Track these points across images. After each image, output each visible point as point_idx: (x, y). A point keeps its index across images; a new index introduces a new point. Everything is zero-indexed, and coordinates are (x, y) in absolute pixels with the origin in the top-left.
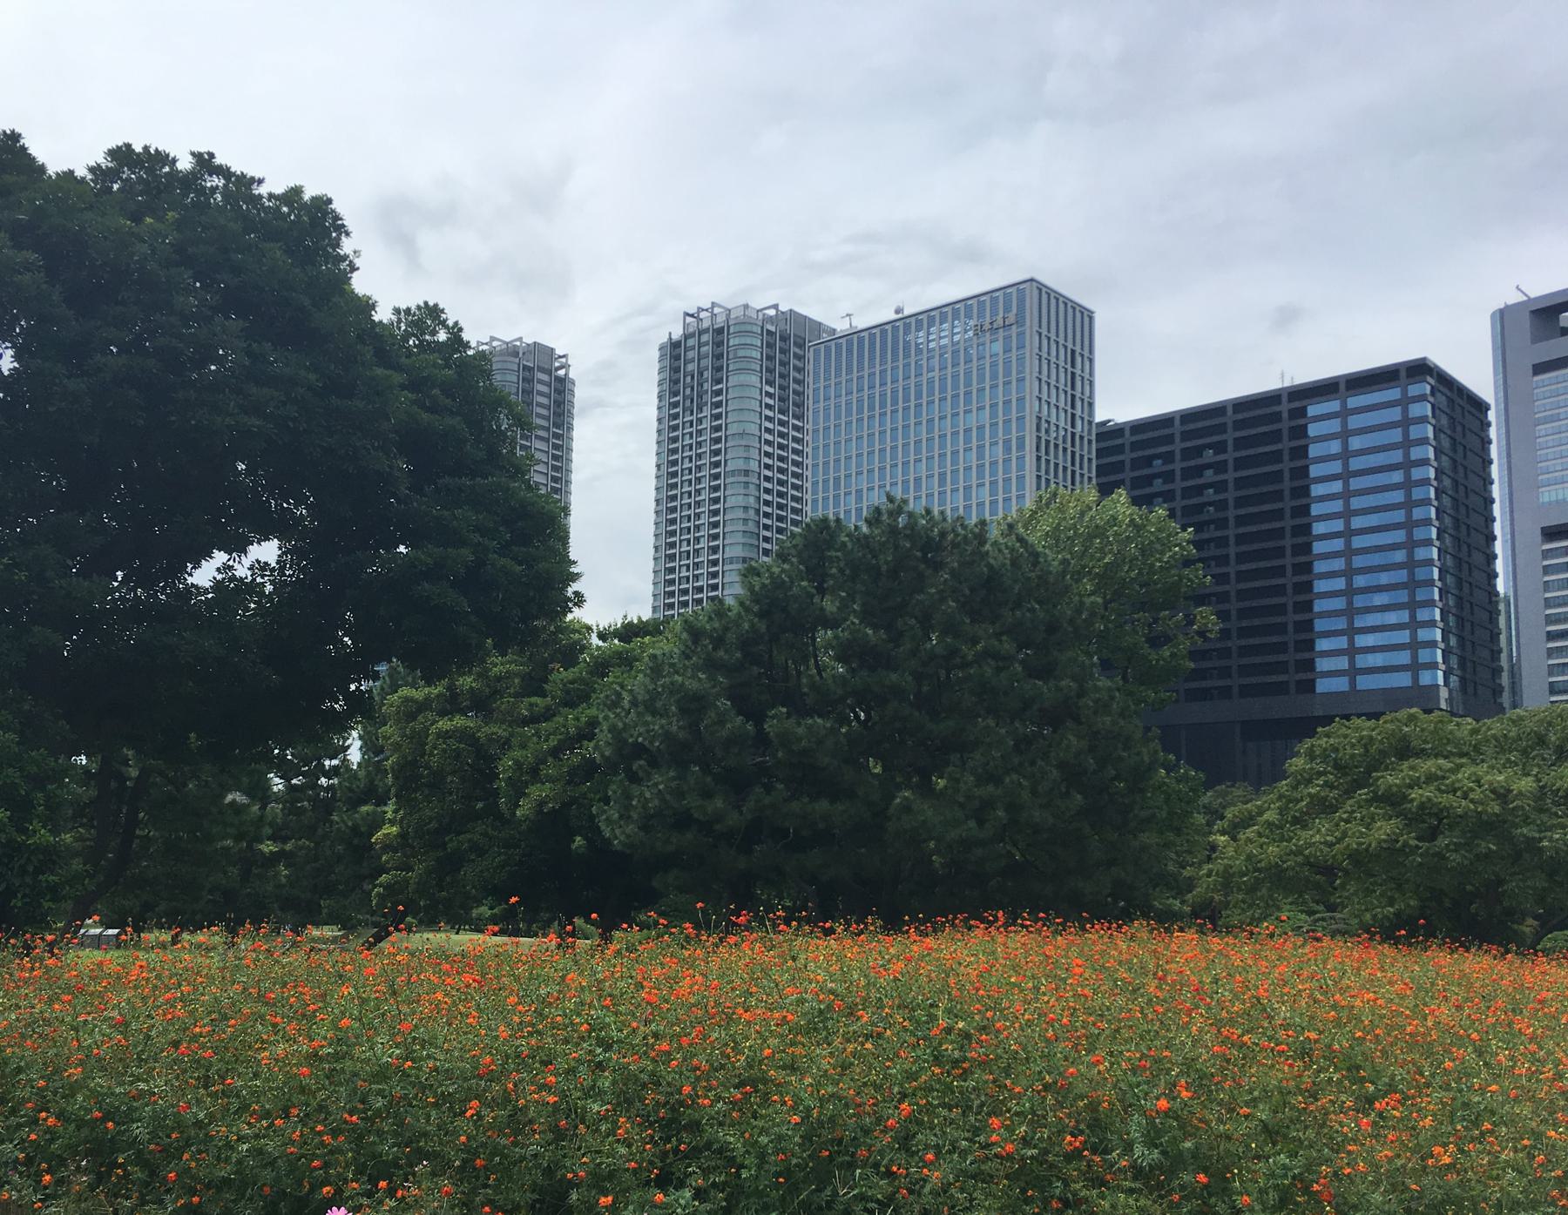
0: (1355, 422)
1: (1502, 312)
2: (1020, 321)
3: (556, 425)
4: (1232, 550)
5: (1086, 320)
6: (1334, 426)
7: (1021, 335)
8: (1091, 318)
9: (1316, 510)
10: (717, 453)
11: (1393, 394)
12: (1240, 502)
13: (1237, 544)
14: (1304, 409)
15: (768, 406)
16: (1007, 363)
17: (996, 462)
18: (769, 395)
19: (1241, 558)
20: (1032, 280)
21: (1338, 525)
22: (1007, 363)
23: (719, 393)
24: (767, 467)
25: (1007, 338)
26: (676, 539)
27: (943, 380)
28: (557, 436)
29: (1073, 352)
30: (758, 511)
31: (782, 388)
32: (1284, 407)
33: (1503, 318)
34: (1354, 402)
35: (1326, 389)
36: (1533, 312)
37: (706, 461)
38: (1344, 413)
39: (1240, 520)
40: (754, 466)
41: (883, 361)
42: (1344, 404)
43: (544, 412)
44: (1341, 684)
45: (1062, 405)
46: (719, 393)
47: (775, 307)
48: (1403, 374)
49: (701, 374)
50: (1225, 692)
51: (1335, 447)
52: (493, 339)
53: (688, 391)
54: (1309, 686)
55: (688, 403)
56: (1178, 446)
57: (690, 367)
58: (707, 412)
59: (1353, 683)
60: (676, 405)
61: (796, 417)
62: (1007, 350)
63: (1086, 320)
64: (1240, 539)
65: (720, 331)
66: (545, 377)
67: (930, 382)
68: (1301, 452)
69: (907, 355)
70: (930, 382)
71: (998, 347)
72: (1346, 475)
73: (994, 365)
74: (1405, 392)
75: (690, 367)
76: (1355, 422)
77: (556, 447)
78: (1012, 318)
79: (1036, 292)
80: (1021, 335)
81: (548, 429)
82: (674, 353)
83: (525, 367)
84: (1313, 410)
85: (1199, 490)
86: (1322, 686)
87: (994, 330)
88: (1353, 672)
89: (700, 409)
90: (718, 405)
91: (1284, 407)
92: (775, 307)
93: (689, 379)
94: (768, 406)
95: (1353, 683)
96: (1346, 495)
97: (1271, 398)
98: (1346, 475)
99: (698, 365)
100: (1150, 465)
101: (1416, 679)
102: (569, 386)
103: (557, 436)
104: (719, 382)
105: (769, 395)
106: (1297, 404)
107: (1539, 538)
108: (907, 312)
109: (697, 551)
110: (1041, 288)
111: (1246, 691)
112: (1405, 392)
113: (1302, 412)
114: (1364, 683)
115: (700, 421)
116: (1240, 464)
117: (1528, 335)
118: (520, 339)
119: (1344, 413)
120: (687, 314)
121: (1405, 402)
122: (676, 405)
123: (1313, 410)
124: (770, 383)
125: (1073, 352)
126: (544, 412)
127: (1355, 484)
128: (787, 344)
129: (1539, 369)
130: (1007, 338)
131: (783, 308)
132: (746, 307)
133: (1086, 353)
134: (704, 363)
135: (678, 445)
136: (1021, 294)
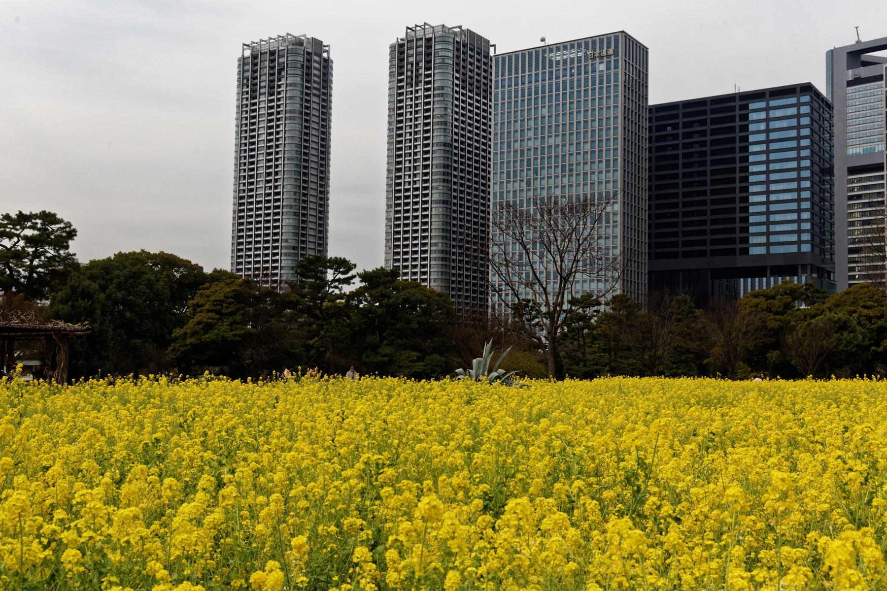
1: (832, 51)
2: (616, 53)
3: (324, 88)
4: (709, 178)
7: (616, 61)
8: (647, 52)
9: (752, 159)
11: (793, 100)
12: (713, 153)
13: (711, 175)
14: (747, 106)
15: (457, 85)
16: (608, 76)
17: (594, 131)
18: (457, 78)
19: (713, 182)
20: (623, 32)
21: (763, 168)
22: (608, 76)
25: (609, 63)
27: (572, 82)
28: (324, 94)
30: (301, 113)
31: (463, 74)
32: (737, 103)
33: (832, 55)
34: (773, 103)
36: (848, 53)
37: (421, 114)
39: (713, 162)
40: (450, 120)
41: (537, 68)
42: (768, 104)
44: (761, 251)
46: (429, 76)
47: (460, 27)
48: (798, 90)
50: (703, 254)
51: (763, 126)
52: (288, 34)
53: (409, 73)
54: (745, 251)
56: (681, 121)
57: (410, 59)
58: (421, 86)
59: (768, 250)
61: (485, 98)
62: (608, 68)
64: (713, 172)
66: (317, 58)
67: (565, 82)
68: (745, 128)
69: (551, 66)
70: (565, 82)
71: (603, 67)
72: (768, 142)
73: (601, 77)
75: (410, 59)
77: (324, 100)
78: (611, 51)
80: (616, 61)
81: (319, 90)
82: (399, 51)
84: (752, 106)
85: (691, 145)
86: (754, 251)
88: (768, 244)
89: (417, 85)
92: (460, 27)
93: (409, 66)
94: (457, 85)
95: (768, 250)
96: (768, 152)
98: (768, 142)
99: (414, 57)
100: (665, 130)
101: (799, 248)
102: (330, 63)
103: (324, 94)
104: (429, 69)
105: (457, 78)
107: (846, 172)
108: (549, 41)
111: (714, 253)
113: (746, 107)
114: (774, 250)
115: (417, 91)
116: (714, 132)
117: (845, 64)
118: (305, 36)
119: (767, 109)
120: (408, 28)
121: (798, 105)
123: (752, 106)
124: (457, 72)
128: (469, 49)
130: (609, 63)
132: (443, 26)
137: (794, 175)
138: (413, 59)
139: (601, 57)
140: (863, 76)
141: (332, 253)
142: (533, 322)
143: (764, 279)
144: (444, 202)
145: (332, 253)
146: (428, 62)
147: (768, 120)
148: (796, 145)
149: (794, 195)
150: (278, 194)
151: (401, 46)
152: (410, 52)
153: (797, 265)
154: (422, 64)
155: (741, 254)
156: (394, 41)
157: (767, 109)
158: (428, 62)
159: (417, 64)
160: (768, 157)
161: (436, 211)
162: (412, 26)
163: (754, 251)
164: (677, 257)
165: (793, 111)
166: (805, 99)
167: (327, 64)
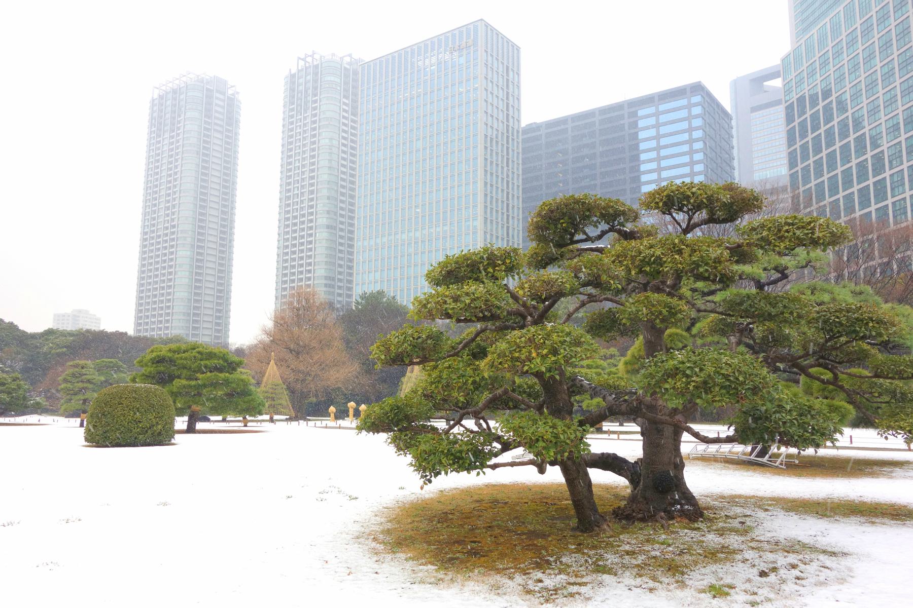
0: (663, 118)
5: (516, 51)
6: (652, 121)
10: (313, 157)
11: (684, 102)
15: (345, 111)
23: (316, 102)
24: (343, 166)
26: (294, 126)
29: (507, 67)
34: (662, 107)
35: (648, 100)
38: (657, 114)
43: (221, 103)
45: (501, 107)
46: (316, 102)
47: (350, 55)
49: (306, 91)
58: (309, 113)
60: (292, 110)
63: (516, 51)
65: (316, 67)
66: (221, 97)
74: (689, 101)
76: (663, 118)
79: (484, 27)
83: (208, 90)
84: (641, 113)
87: (460, 49)
89: (305, 112)
90: (315, 108)
92: (350, 55)
94: (345, 111)
97: (619, 107)
104: (316, 95)
105: (345, 104)
106: (633, 109)
109: (302, 193)
110: (487, 25)
112: (689, 101)
113: (635, 114)
115: (305, 118)
119: (657, 114)
120: (299, 58)
121: (689, 107)
122: (292, 110)
123: (641, 113)
124: (345, 97)
125: (507, 67)
126: (221, 103)
127: (663, 153)
129: (754, 109)
131: (355, 56)
133: (515, 69)
134: (308, 78)
135: (293, 153)
136: (476, 28)
137: (685, 148)
138: (302, 88)
140: (702, 434)
144: (328, 227)
146: (315, 88)
147: (657, 126)
148: (689, 172)
149: (685, 125)
150: (174, 227)
151: (293, 76)
152: (301, 81)
154: (310, 92)
158: (315, 88)
159: (306, 91)
160: (659, 164)
161: (322, 235)
162: (303, 56)
165: (683, 114)
166: (697, 99)
167: (232, 105)
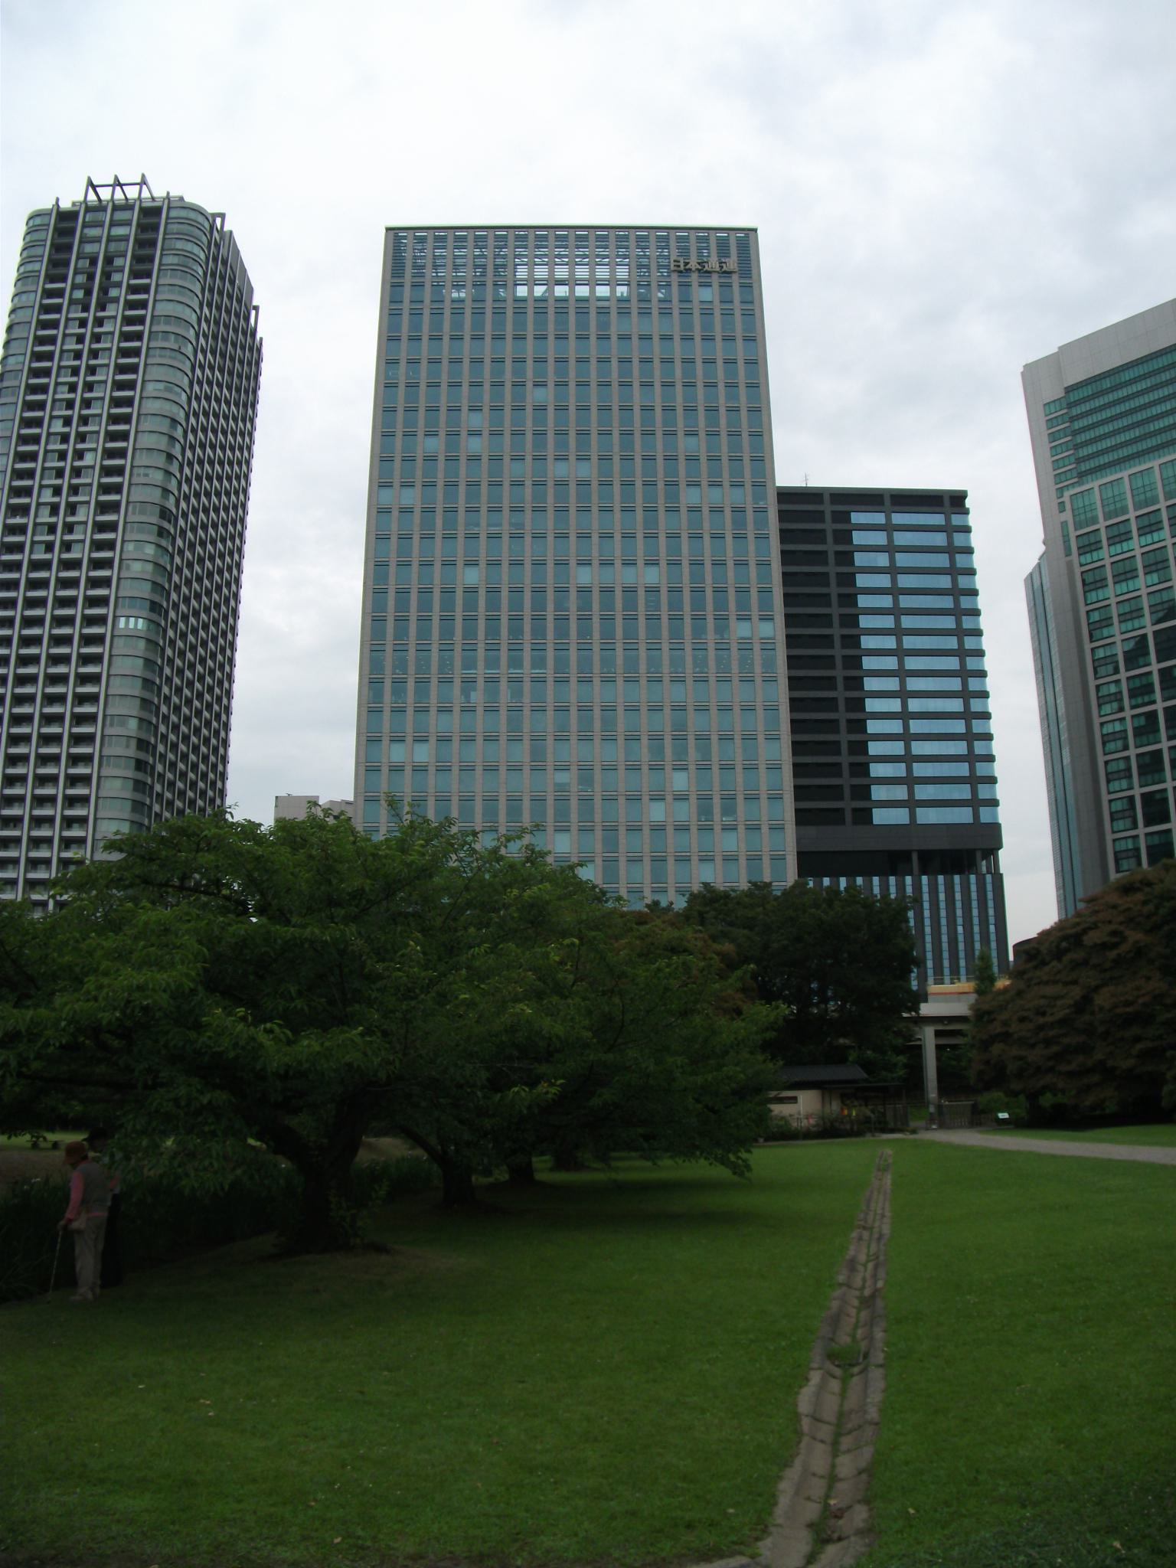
34: (898, 518)
44: (900, 816)
54: (864, 816)
55: (79, 294)
65: (156, 212)
84: (857, 518)
86: (880, 816)
91: (828, 508)
93: (85, 264)
95: (913, 816)
100: (123, 724)
113: (845, 517)
114: (928, 816)
123: (857, 518)
139: (703, 271)
141: (255, 303)
142: (35, 897)
143: (908, 879)
145: (255, 303)
153: (974, 851)
155: (855, 822)
156: (48, 204)
157: (889, 528)
163: (880, 816)
164: (841, 821)
